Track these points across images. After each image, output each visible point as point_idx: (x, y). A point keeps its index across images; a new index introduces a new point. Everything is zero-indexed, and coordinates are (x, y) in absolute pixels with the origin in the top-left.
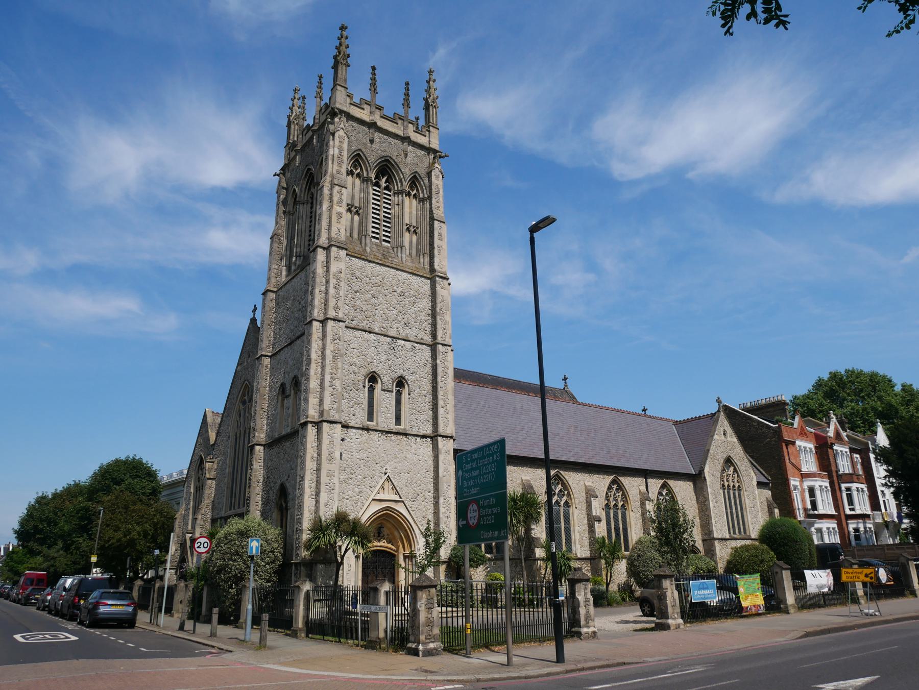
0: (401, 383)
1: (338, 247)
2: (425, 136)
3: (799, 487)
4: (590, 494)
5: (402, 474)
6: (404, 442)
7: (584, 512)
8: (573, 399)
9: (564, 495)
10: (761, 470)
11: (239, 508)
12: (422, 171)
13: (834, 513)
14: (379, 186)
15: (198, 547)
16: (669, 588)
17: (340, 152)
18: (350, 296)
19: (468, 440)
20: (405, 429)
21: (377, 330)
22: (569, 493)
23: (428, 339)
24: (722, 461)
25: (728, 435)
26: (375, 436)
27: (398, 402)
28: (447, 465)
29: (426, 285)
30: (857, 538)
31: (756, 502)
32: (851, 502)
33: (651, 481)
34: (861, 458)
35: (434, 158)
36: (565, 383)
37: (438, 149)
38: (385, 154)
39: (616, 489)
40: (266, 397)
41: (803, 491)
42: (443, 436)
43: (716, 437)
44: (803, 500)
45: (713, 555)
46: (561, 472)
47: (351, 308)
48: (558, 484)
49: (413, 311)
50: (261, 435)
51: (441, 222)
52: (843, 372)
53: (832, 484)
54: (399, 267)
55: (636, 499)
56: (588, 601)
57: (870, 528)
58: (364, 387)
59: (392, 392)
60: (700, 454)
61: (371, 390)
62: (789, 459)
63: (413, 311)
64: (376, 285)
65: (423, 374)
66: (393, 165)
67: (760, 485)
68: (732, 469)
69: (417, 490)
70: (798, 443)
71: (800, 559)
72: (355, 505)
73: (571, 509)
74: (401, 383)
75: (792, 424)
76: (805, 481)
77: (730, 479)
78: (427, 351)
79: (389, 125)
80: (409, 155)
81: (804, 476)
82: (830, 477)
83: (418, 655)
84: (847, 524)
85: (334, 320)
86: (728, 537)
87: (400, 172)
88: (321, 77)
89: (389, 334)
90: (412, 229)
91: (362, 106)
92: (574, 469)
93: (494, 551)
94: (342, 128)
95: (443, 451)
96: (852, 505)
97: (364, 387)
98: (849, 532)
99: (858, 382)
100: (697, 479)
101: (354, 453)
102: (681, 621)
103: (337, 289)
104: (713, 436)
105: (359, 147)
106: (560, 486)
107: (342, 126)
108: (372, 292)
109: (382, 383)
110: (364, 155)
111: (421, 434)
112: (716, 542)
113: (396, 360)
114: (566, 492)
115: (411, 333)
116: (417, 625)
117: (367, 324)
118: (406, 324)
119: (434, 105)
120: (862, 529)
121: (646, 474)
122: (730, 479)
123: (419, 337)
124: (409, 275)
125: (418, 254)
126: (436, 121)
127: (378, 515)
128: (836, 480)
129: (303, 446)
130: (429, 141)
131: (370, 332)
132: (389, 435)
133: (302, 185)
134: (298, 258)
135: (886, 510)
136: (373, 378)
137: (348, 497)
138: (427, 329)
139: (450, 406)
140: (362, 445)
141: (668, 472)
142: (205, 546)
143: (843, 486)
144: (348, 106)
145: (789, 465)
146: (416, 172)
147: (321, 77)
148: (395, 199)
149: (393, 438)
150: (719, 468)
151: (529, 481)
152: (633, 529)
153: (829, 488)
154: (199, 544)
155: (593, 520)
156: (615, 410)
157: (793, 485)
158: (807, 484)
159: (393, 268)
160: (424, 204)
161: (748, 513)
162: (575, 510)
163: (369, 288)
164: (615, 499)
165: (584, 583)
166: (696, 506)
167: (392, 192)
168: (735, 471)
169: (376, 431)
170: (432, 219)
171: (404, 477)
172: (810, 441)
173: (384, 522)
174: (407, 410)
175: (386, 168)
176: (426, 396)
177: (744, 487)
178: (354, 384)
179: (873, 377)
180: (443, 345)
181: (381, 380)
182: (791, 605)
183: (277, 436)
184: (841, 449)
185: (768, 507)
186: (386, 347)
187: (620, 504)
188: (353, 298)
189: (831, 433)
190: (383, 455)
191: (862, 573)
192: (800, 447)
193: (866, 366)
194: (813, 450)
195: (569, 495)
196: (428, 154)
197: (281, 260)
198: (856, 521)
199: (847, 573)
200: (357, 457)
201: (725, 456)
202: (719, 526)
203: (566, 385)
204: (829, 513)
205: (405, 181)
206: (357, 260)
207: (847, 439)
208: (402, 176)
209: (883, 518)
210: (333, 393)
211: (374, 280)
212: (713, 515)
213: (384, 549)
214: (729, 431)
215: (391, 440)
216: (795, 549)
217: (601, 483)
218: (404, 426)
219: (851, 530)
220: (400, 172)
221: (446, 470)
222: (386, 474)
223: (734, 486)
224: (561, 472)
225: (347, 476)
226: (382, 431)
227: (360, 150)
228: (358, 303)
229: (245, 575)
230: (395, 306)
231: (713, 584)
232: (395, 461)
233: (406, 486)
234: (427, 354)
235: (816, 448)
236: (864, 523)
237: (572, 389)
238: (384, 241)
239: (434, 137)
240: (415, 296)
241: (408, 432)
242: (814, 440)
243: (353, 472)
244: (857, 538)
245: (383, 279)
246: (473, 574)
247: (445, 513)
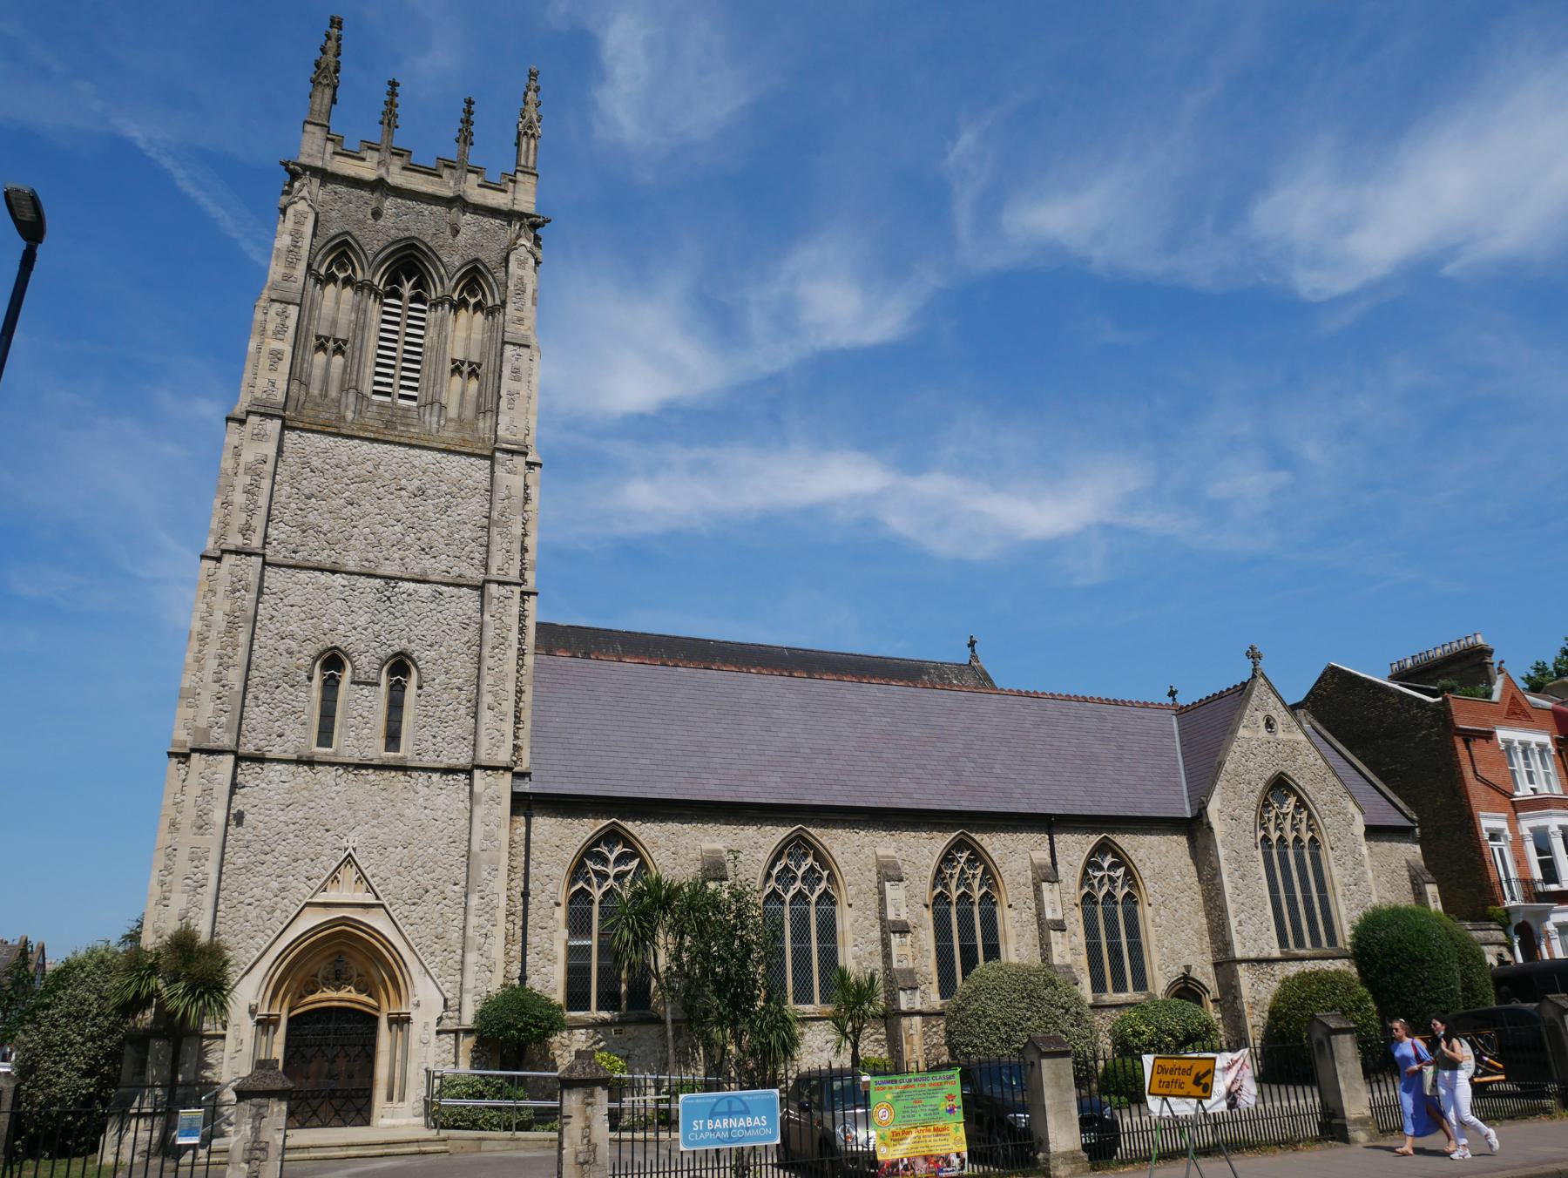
1: (262, 415)
3: (1507, 832)
4: (889, 873)
5: (390, 849)
6: (400, 786)
9: (820, 879)
10: (1396, 800)
12: (490, 256)
14: (400, 297)
16: (575, 1114)
17: (295, 244)
18: (293, 506)
21: (351, 567)
24: (1261, 785)
26: (326, 775)
27: (395, 706)
28: (492, 826)
31: (1364, 873)
33: (1064, 840)
36: (973, 651)
38: (407, 234)
39: (968, 860)
41: (1518, 843)
42: (486, 768)
43: (1242, 732)
44: (1521, 861)
45: (1236, 998)
46: (811, 830)
47: (294, 529)
48: (806, 855)
51: (520, 345)
54: (414, 442)
55: (1022, 880)
56: (262, 1149)
58: (310, 679)
59: (377, 684)
60: (1204, 772)
61: (331, 686)
62: (1475, 772)
64: (357, 480)
67: (1374, 832)
68: (1292, 800)
69: (425, 880)
70: (1502, 734)
71: (1434, 1001)
72: (266, 917)
74: (400, 665)
75: (1488, 695)
76: (1523, 818)
77: (1287, 825)
79: (420, 181)
85: (237, 553)
86: (1276, 953)
87: (438, 264)
89: (380, 572)
90: (466, 369)
92: (849, 821)
93: (624, 1003)
95: (484, 799)
100: (1194, 828)
101: (274, 812)
103: (253, 494)
104: (1235, 731)
105: (347, 228)
106: (810, 860)
108: (347, 494)
111: (442, 766)
112: (1241, 970)
113: (392, 622)
114: (825, 874)
115: (435, 567)
118: (423, 550)
119: (530, 132)
122: (1287, 825)
123: (455, 571)
127: (319, 935)
131: (334, 572)
132: (363, 772)
136: (333, 661)
137: (250, 900)
138: (477, 555)
145: (1473, 786)
146: (477, 260)
148: (431, 316)
149: (372, 777)
150: (1254, 799)
157: (1487, 830)
158: (1526, 825)
159: (400, 444)
161: (1340, 900)
162: (1009, 913)
163: (339, 487)
164: (963, 881)
166: (1197, 887)
168: (1301, 804)
172: (1540, 728)
177: (1327, 840)
180: (500, 583)
181: (352, 663)
182: (1064, 1155)
185: (1412, 882)
188: (301, 510)
190: (344, 812)
192: (1509, 743)
194: (1550, 746)
195: (832, 878)
196: (510, 225)
200: (282, 819)
201: (1269, 774)
202: (1249, 930)
203: (974, 656)
208: (442, 271)
210: (220, 695)
211: (353, 471)
212: (1231, 908)
213: (348, 1004)
216: (1420, 979)
217: (924, 849)
220: (438, 264)
221: (489, 837)
223: (1297, 840)
224: (811, 830)
225: (253, 859)
226: (345, 766)
228: (312, 518)
229: (39, 1061)
230: (399, 517)
231: (771, 1101)
233: (399, 874)
234: (470, 604)
235: (1557, 742)
237: (987, 663)
239: (526, 190)
240: (450, 493)
241: (409, 764)
242: (1552, 725)
243: (267, 849)
246: (561, 1056)
247: (481, 926)
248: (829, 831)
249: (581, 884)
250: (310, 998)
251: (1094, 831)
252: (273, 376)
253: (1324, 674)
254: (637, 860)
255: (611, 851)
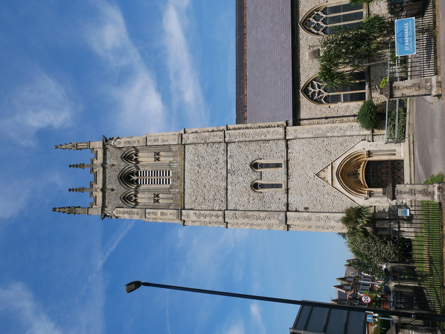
1: (181, 216)
6: (293, 162)
9: (318, 14)
12: (119, 153)
14: (138, 180)
15: (368, 301)
18: (208, 203)
19: (286, 107)
26: (291, 184)
27: (267, 166)
28: (304, 131)
42: (285, 135)
47: (215, 202)
48: (309, 21)
49: (208, 157)
54: (183, 170)
56: (411, 191)
58: (261, 192)
59: (261, 172)
61: (263, 186)
63: (208, 157)
64: (197, 185)
65: (246, 148)
66: (122, 173)
69: (323, 150)
73: (328, 6)
74: (254, 166)
80: (112, 163)
85: (224, 218)
87: (125, 169)
89: (225, 175)
91: (95, 197)
94: (112, 212)
95: (296, 135)
101: (304, 199)
103: (206, 215)
105: (119, 198)
106: (311, 19)
107: (110, 212)
108: (202, 188)
109: (257, 180)
110: (122, 195)
113: (241, 170)
114: (316, 13)
117: (222, 191)
118: (217, 163)
123: (223, 152)
124: (186, 161)
126: (85, 143)
131: (227, 189)
132: (289, 173)
138: (217, 146)
140: (298, 193)
142: (367, 298)
144: (97, 207)
149: (291, 171)
151: (309, 53)
154: (365, 301)
159: (184, 174)
163: (200, 191)
165: (396, 194)
171: (316, 162)
173: (346, 174)
176: (260, 146)
178: (261, 200)
180: (225, 138)
186: (234, 177)
188: (209, 201)
190: (302, 178)
195: (317, 10)
196: (108, 148)
205: (129, 165)
206: (186, 200)
208: (127, 168)
210: (269, 218)
211: (195, 187)
218: (282, 161)
220: (125, 169)
225: (319, 203)
227: (120, 198)
230: (207, 171)
232: (305, 168)
233: (321, 159)
234: (233, 146)
238: (169, 175)
240: (198, 157)
245: (192, 180)
246: (381, 100)
248: (300, 13)
249: (322, 100)
250: (362, 182)
251: (298, 27)
252: (169, 214)
254: (314, 82)
255: (311, 91)
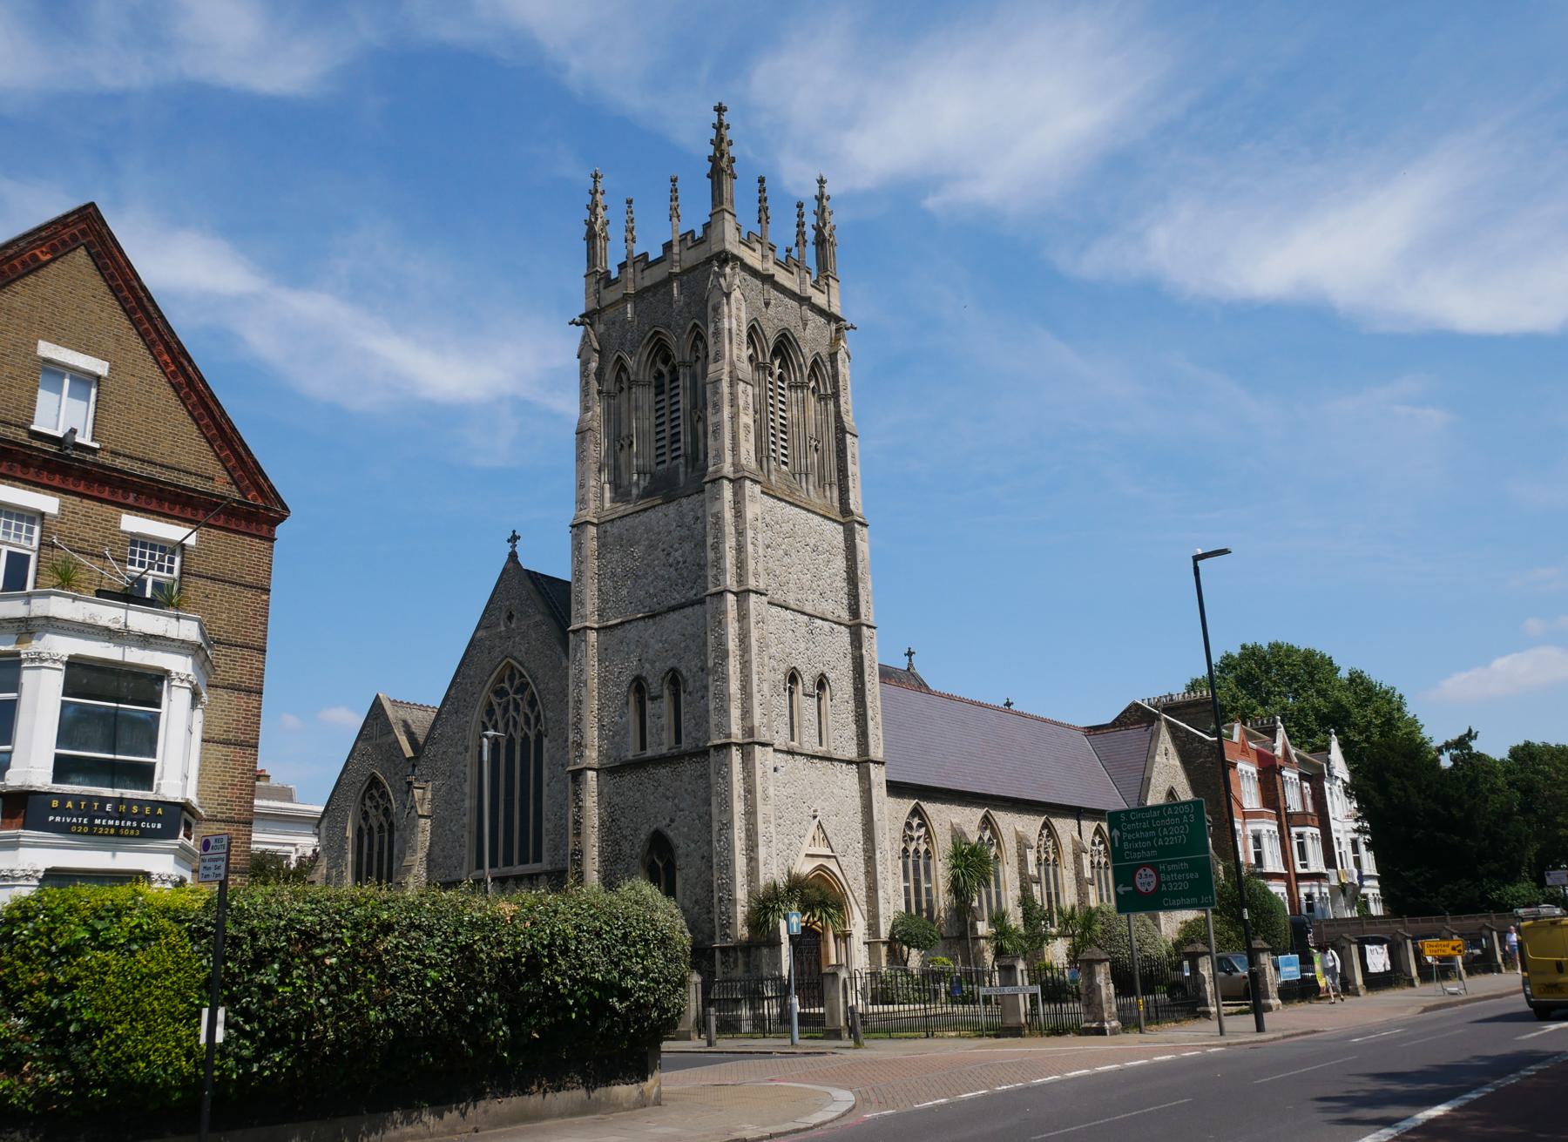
0: (822, 682)
1: (752, 480)
2: (823, 293)
7: (1016, 869)
8: (921, 686)
9: (992, 844)
11: (508, 862)
12: (824, 354)
13: (1283, 871)
20: (829, 752)
22: (998, 843)
23: (845, 616)
25: (1170, 755)
29: (835, 533)
30: (1310, 908)
32: (1303, 856)
34: (1312, 788)
35: (838, 330)
36: (910, 660)
37: (839, 314)
40: (595, 693)
43: (1157, 758)
50: (592, 756)
52: (1265, 647)
53: (1280, 827)
54: (810, 508)
57: (1325, 894)
70: (1240, 765)
74: (822, 682)
78: (844, 636)
81: (1247, 815)
82: (1278, 817)
83: (1106, 1034)
84: (1298, 887)
85: (756, 593)
88: (674, 180)
91: (752, 245)
96: (1305, 860)
97: (785, 690)
98: (1299, 898)
99: (1288, 664)
102: (1280, 1002)
104: (1154, 757)
116: (1097, 1001)
120: (1317, 895)
121: (1078, 813)
125: (822, 484)
128: (1286, 821)
129: (723, 778)
130: (829, 301)
131: (787, 608)
133: (641, 355)
134: (642, 475)
135: (1342, 867)
136: (793, 677)
138: (844, 601)
139: (879, 718)
141: (1051, 804)
143: (1294, 831)
147: (674, 180)
149: (818, 765)
152: (1067, 894)
153: (1277, 833)
155: (1028, 881)
156: (972, 703)
160: (826, 405)
167: (786, 383)
169: (801, 754)
170: (841, 431)
172: (1252, 762)
174: (830, 723)
175: (784, 347)
179: (1309, 656)
183: (631, 758)
184: (1290, 774)
187: (1052, 857)
189: (1279, 752)
191: (1448, 946)
193: (1302, 641)
194: (1256, 775)
197: (600, 471)
198: (1308, 883)
199: (1431, 946)
203: (910, 664)
204: (1278, 871)
207: (1296, 760)
209: (1339, 880)
214: (1172, 749)
215: (817, 768)
217: (1030, 825)
219: (1302, 896)
222: (815, 817)
235: (1258, 772)
236: (1320, 886)
237: (919, 669)
244: (1310, 908)
251: (981, 806)
253: (1130, 708)
